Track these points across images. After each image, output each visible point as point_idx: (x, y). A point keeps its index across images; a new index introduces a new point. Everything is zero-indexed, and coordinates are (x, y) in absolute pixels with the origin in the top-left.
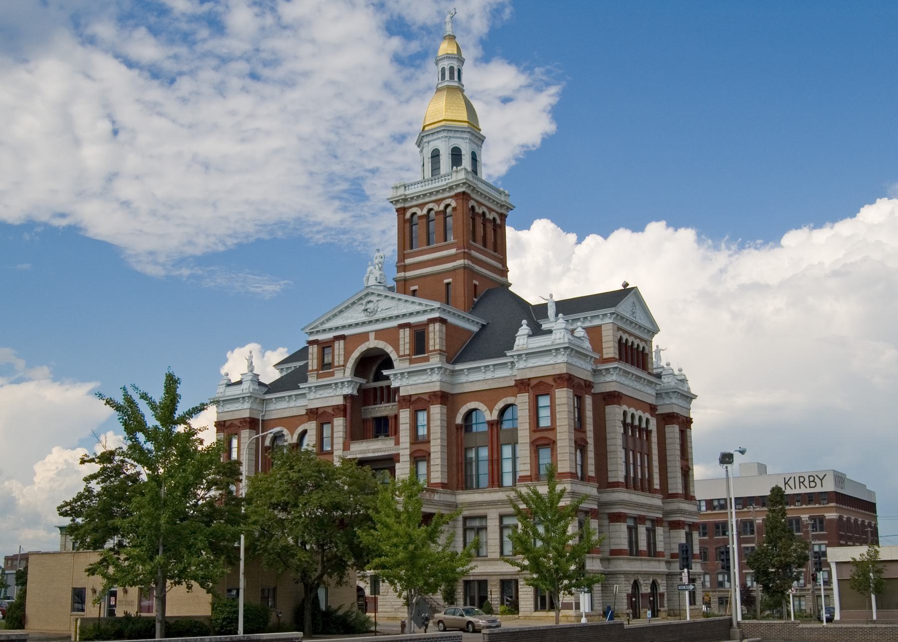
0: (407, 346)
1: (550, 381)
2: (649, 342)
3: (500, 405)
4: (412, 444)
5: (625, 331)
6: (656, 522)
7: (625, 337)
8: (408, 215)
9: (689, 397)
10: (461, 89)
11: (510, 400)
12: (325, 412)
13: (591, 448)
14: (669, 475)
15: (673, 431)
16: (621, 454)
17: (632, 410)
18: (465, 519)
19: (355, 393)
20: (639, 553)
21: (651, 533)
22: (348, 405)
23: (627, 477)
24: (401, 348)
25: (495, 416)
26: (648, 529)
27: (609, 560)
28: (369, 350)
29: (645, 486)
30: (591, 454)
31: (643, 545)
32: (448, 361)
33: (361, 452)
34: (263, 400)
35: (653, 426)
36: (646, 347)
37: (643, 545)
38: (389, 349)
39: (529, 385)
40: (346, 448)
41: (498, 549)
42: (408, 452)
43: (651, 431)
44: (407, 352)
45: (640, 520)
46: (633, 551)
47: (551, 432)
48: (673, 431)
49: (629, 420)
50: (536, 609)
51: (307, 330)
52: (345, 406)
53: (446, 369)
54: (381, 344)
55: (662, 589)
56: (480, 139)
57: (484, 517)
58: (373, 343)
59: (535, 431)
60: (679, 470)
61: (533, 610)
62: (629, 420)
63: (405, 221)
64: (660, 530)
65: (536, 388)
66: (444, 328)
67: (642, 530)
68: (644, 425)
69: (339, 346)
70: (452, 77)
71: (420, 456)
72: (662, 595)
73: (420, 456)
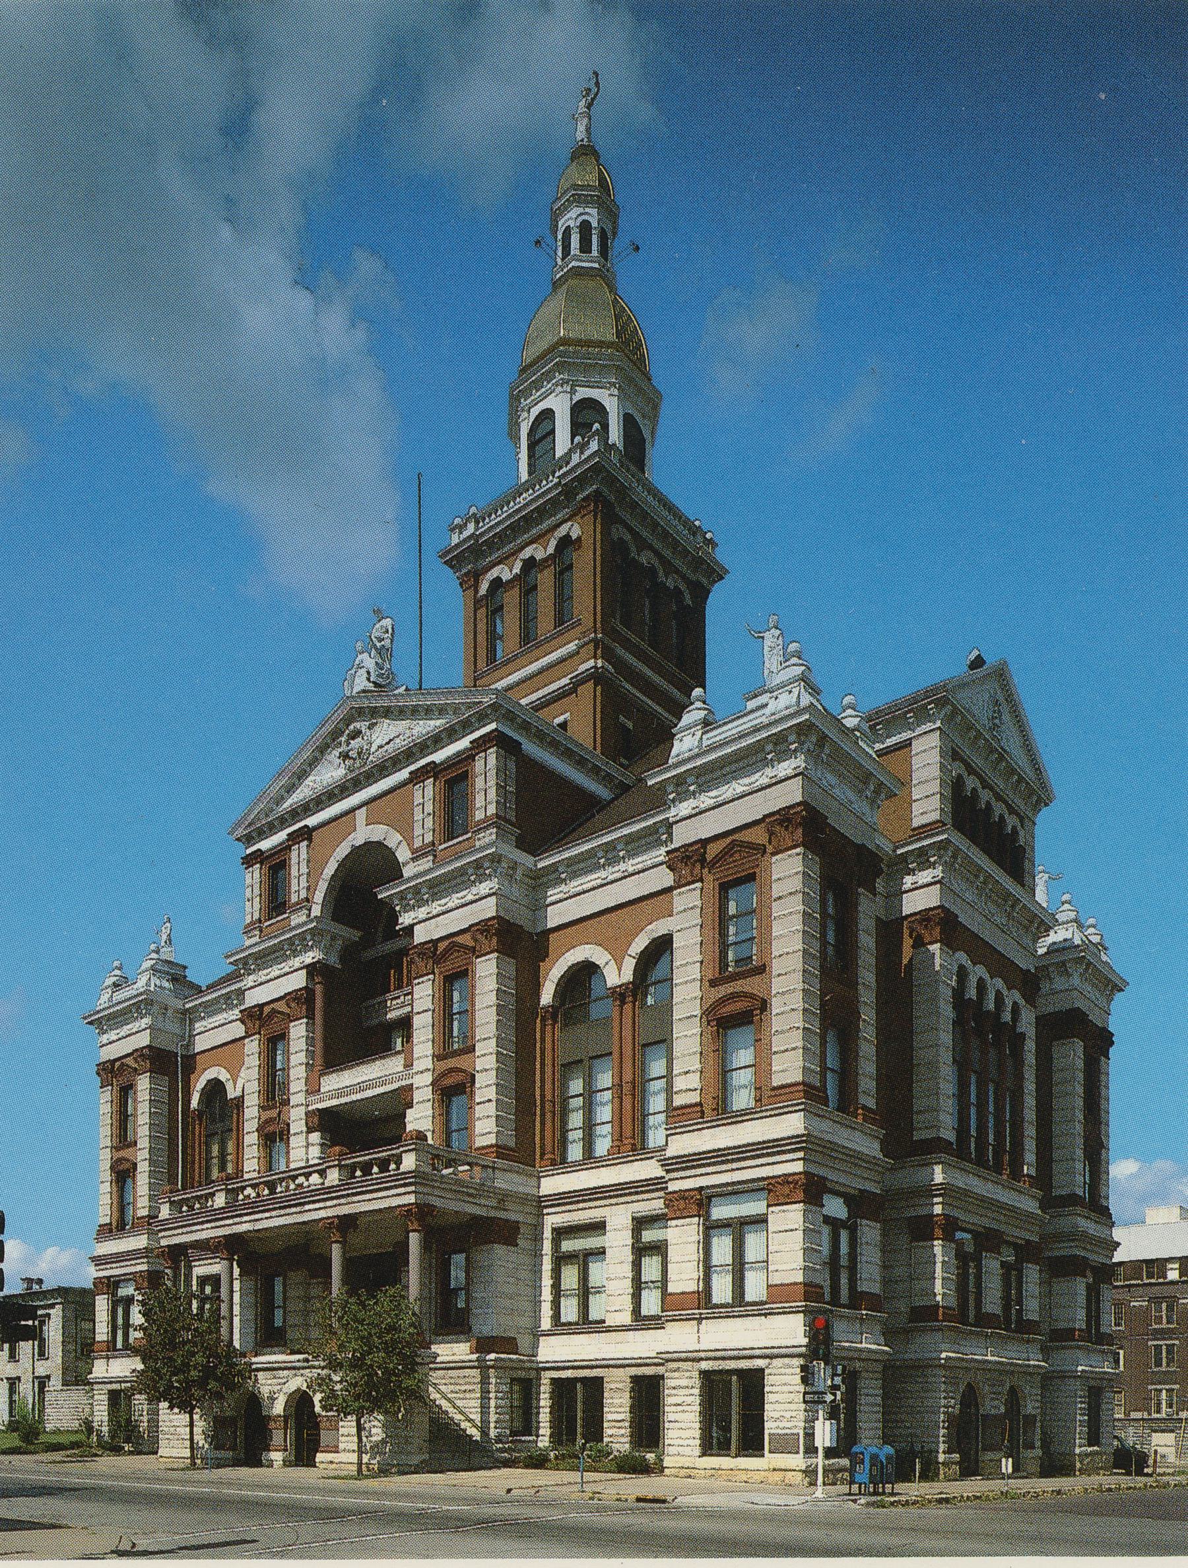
0: (429, 823)
1: (758, 836)
2: (1026, 821)
3: (640, 944)
4: (438, 1057)
5: (971, 770)
6: (1026, 1252)
7: (971, 782)
8: (484, 588)
9: (1111, 985)
10: (604, 275)
11: (659, 928)
12: (274, 1011)
13: (868, 1032)
14: (1055, 1155)
15: (1072, 1054)
16: (947, 1072)
17: (980, 971)
18: (561, 1233)
19: (334, 960)
20: (984, 1320)
21: (1012, 1275)
22: (319, 989)
23: (962, 1130)
24: (418, 831)
25: (628, 975)
26: (1003, 1265)
27: (906, 1331)
28: (356, 850)
29: (1000, 1160)
30: (867, 1048)
31: (992, 1303)
32: (523, 844)
33: (340, 1092)
34: (186, 1012)
35: (1027, 1024)
36: (1022, 833)
37: (992, 1303)
38: (393, 839)
39: (702, 861)
40: (313, 1090)
41: (627, 1302)
42: (428, 1078)
43: (1023, 1035)
44: (429, 838)
45: (988, 1240)
46: (967, 1315)
47: (757, 978)
48: (1072, 1054)
49: (972, 993)
50: (704, 1454)
51: (240, 832)
52: (308, 990)
53: (514, 866)
54: (377, 833)
55: (1031, 1407)
56: (650, 400)
57: (599, 1227)
58: (364, 832)
59: (713, 983)
60: (1080, 1141)
61: (697, 1451)
62: (972, 993)
63: (477, 603)
64: (1032, 1274)
65: (726, 867)
66: (512, 766)
67: (992, 1265)
68: (1007, 1017)
69: (299, 855)
70: (585, 247)
71: (453, 1090)
72: (1030, 1420)
73: (453, 1090)
